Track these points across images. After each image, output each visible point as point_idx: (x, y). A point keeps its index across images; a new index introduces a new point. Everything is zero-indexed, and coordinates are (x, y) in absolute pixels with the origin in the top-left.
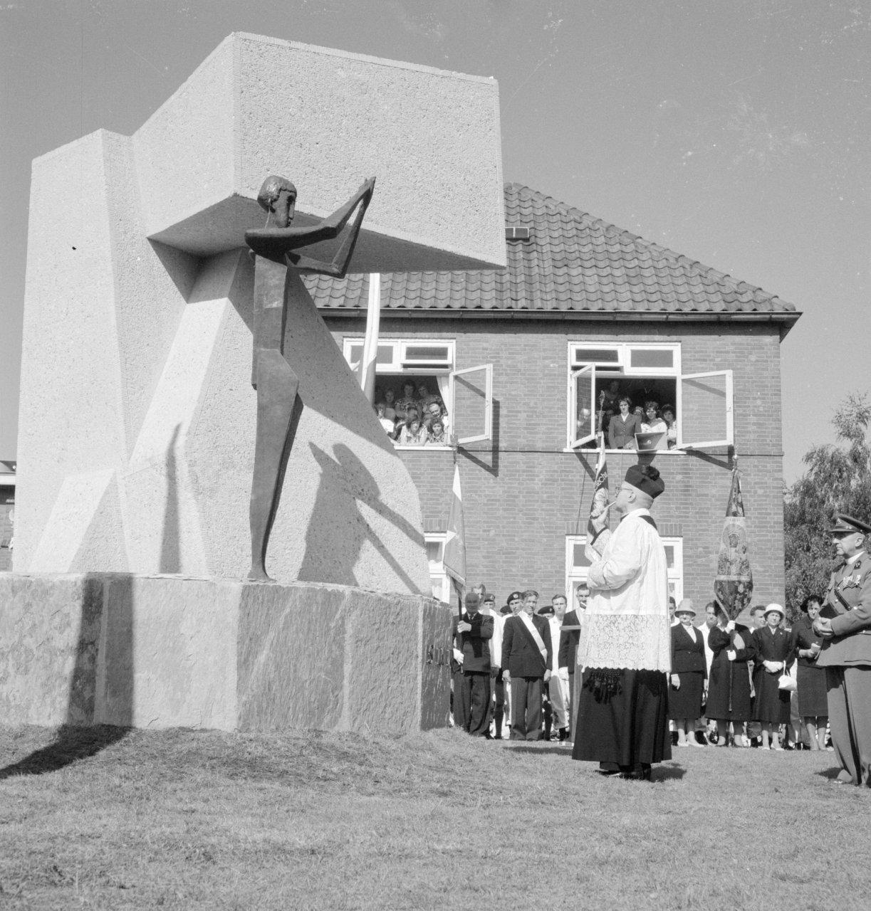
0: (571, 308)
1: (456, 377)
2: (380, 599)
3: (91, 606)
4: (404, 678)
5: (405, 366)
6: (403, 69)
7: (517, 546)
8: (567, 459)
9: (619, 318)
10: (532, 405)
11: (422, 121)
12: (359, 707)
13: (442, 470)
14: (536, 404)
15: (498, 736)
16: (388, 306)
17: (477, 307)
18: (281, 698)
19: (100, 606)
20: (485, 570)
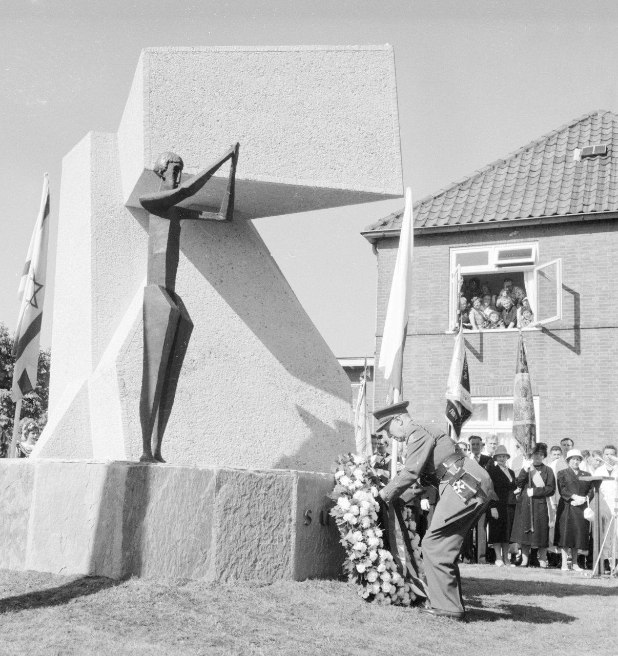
0: (556, 214)
5: (500, 266)
6: (298, 52)
7: (594, 405)
8: (437, 352)
9: (544, 222)
10: (604, 289)
11: (317, 89)
12: (227, 561)
16: (482, 221)
17: (580, 212)
18: (157, 553)
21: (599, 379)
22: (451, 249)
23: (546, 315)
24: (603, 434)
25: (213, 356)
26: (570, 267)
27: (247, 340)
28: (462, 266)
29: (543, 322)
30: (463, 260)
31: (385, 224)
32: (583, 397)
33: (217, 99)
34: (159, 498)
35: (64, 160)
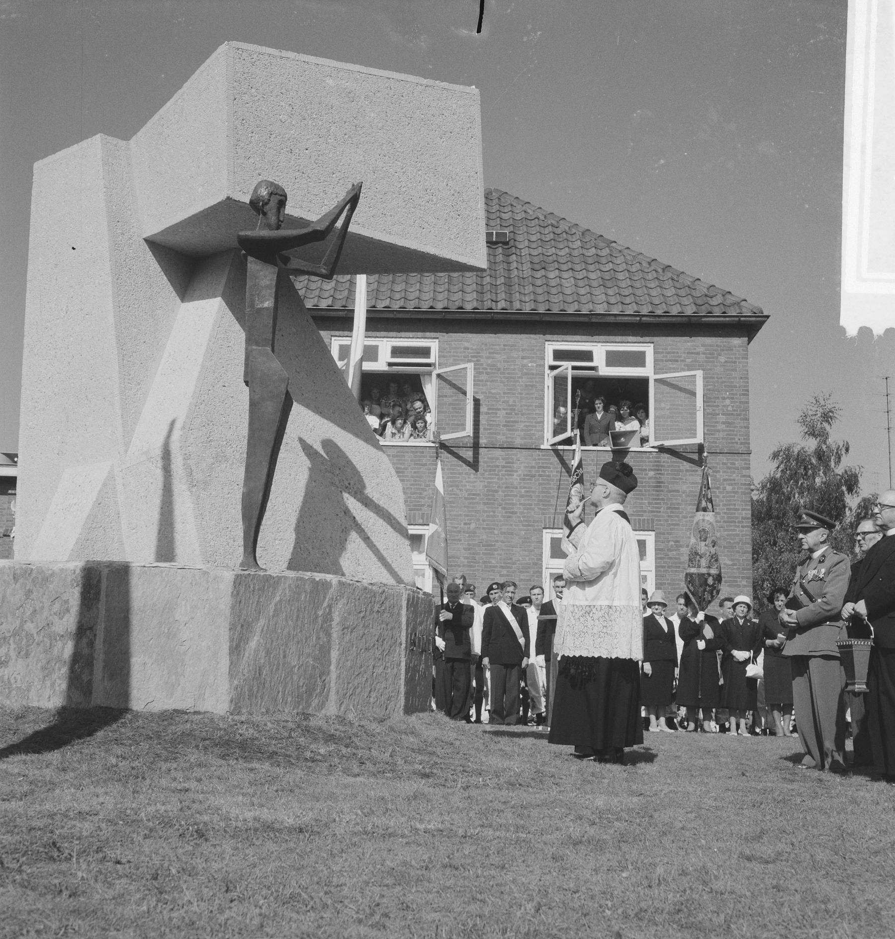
0: (549, 310)
2: (366, 589)
5: (390, 365)
10: (511, 403)
13: (426, 465)
14: (514, 401)
15: (478, 720)
18: (271, 682)
24: (505, 572)
32: (484, 528)
33: (306, 122)
34: (271, 614)
35: (36, 165)
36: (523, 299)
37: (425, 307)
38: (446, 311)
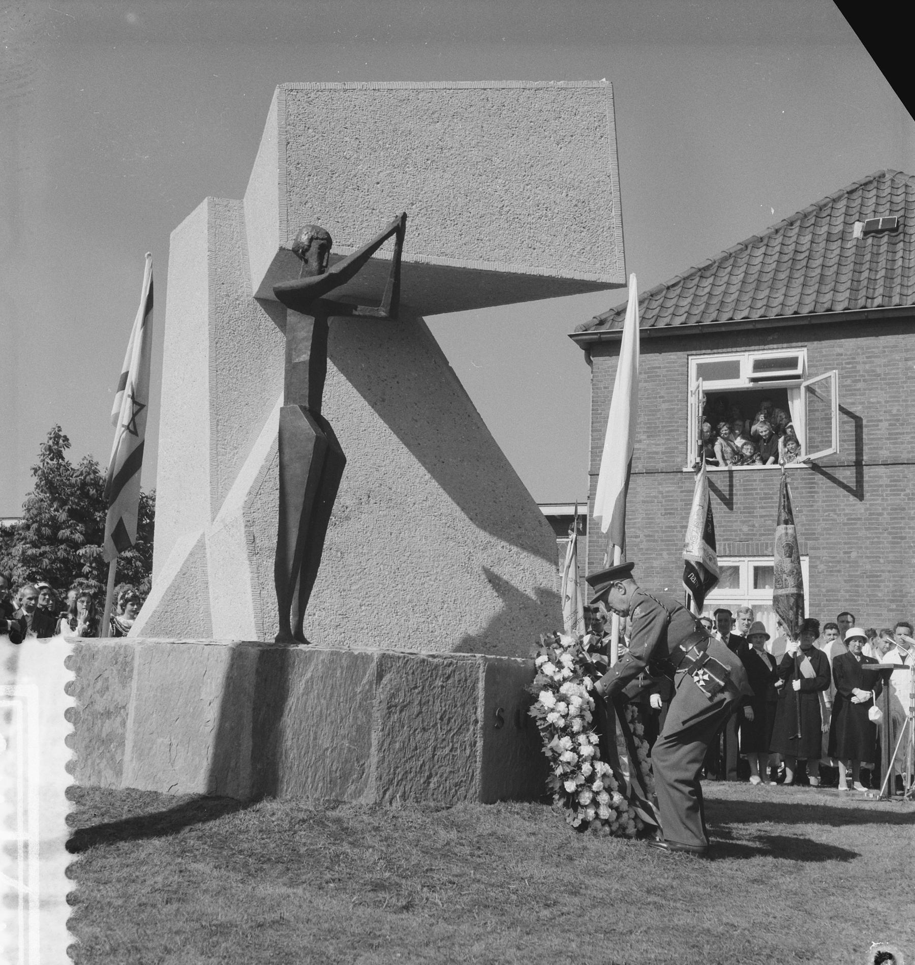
1: (809, 389)
2: (423, 661)
3: (125, 670)
4: (457, 745)
5: (754, 380)
6: (485, 89)
7: (882, 568)
9: (814, 321)
10: (894, 412)
12: (391, 776)
14: (898, 410)
17: (827, 311)
18: (298, 766)
19: (132, 671)
20: (847, 596)
21: (890, 533)
22: (690, 358)
23: (818, 447)
24: (894, 607)
25: (372, 501)
26: (849, 382)
27: (417, 481)
28: (704, 380)
29: (813, 457)
30: (705, 372)
31: (602, 323)
32: (867, 557)
36: (905, 292)
37: (788, 313)
38: (812, 316)
